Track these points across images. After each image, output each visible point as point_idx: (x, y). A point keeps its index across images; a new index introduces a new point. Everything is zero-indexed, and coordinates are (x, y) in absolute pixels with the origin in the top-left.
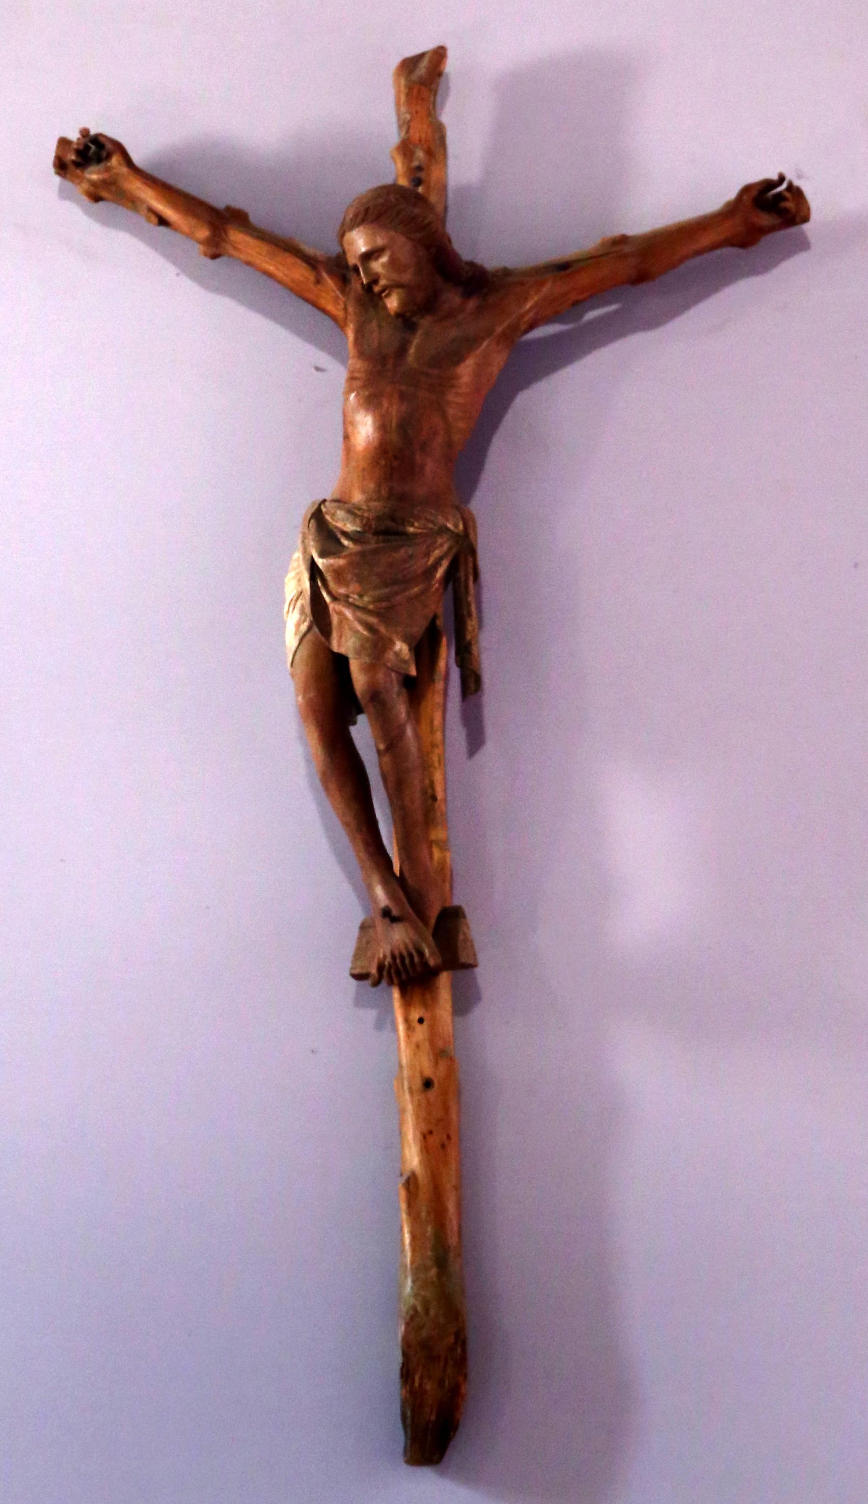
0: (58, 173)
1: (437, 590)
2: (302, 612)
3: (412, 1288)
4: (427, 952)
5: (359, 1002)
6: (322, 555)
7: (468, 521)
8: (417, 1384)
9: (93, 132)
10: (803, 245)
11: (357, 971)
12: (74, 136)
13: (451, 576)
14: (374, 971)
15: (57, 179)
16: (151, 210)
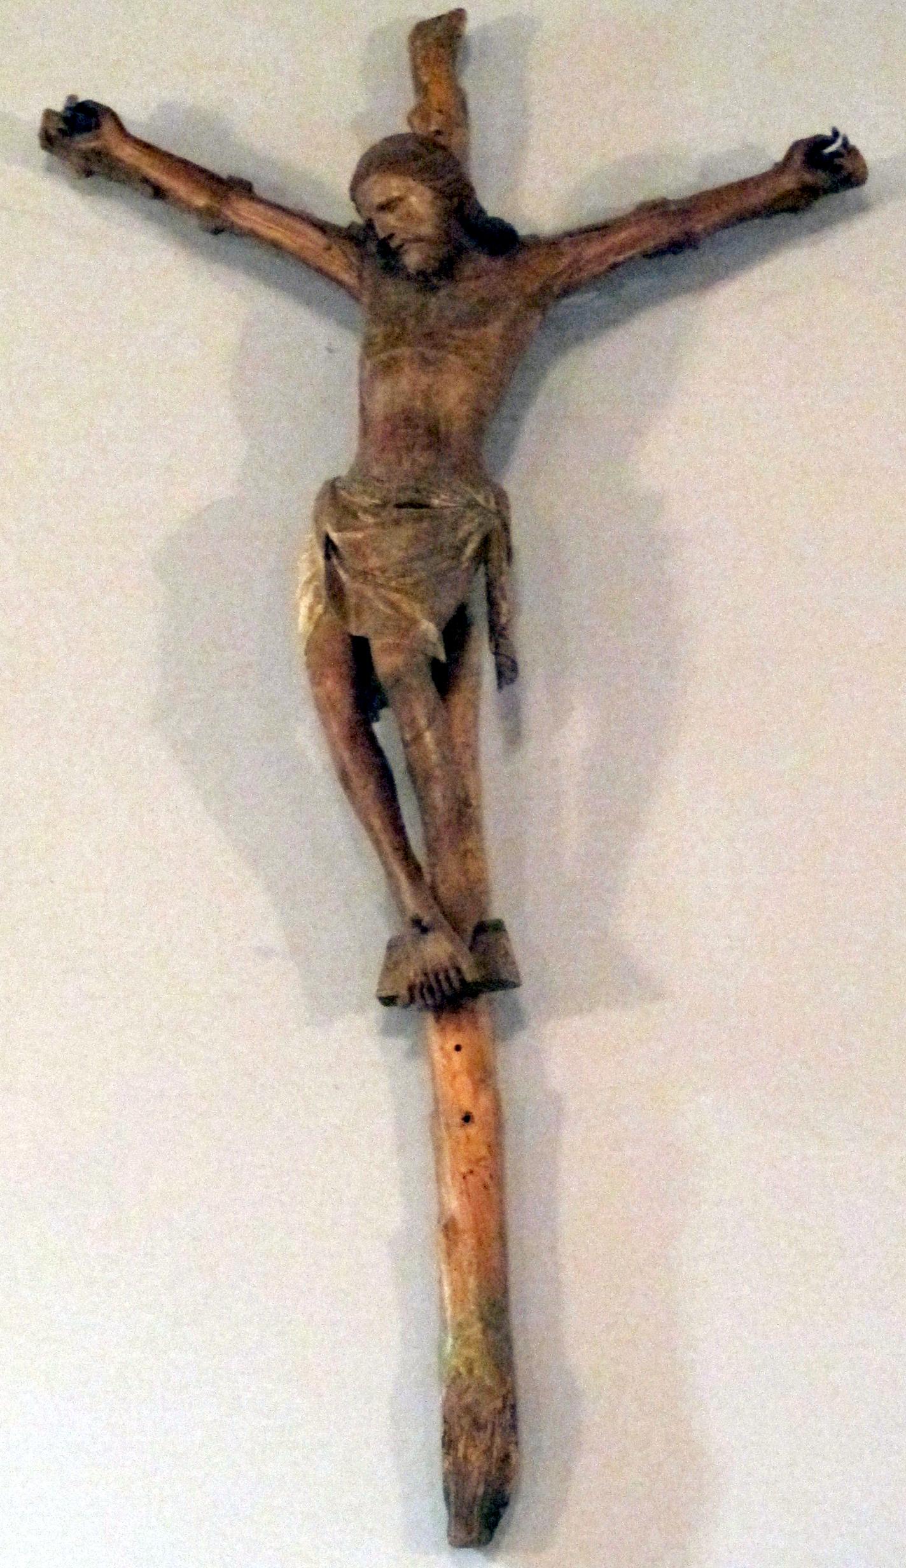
0: (44, 147)
1: (468, 568)
2: (317, 595)
3: (453, 1346)
4: (464, 967)
5: (388, 1030)
6: (339, 530)
7: (501, 497)
8: (460, 1454)
9: (82, 98)
10: (863, 207)
11: (384, 994)
12: (59, 106)
13: (483, 555)
14: (404, 992)
15: (43, 154)
16: (145, 180)
